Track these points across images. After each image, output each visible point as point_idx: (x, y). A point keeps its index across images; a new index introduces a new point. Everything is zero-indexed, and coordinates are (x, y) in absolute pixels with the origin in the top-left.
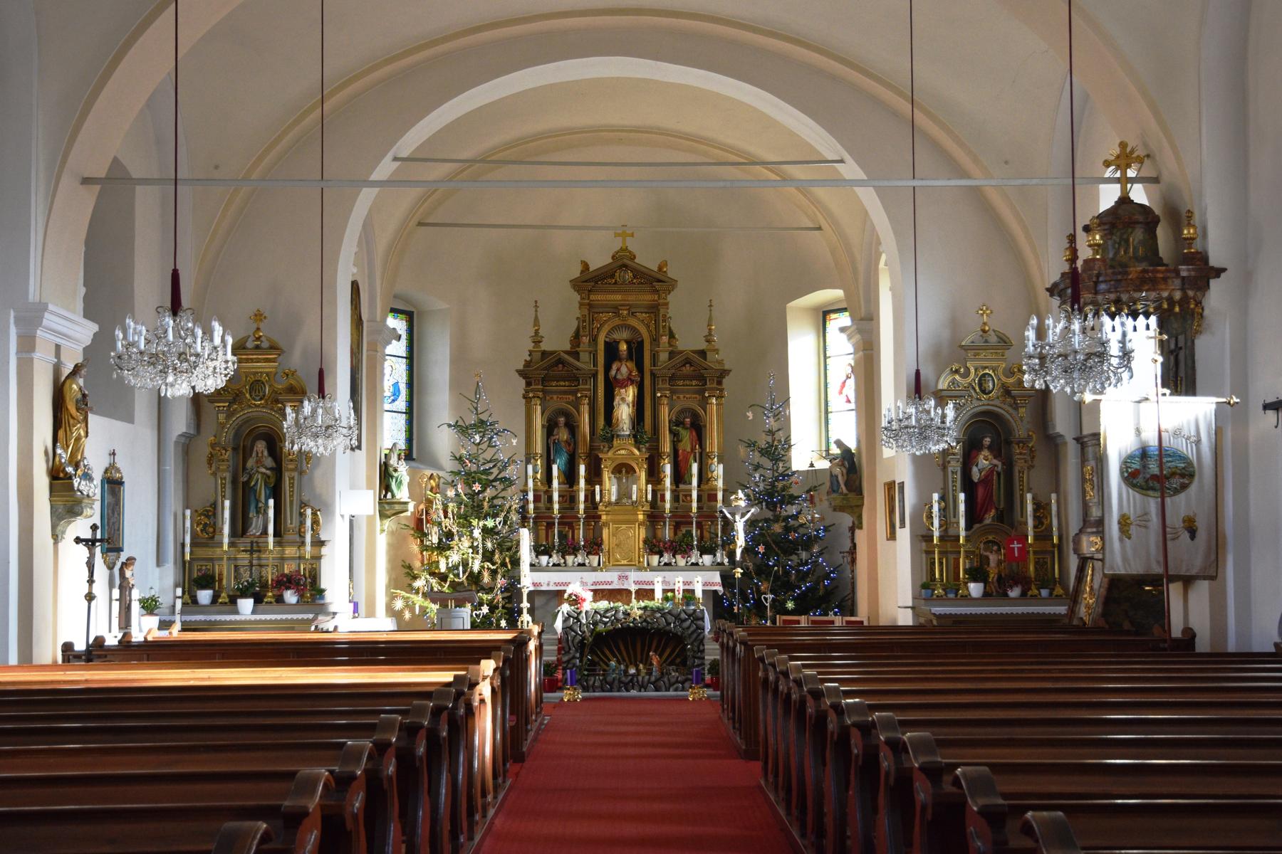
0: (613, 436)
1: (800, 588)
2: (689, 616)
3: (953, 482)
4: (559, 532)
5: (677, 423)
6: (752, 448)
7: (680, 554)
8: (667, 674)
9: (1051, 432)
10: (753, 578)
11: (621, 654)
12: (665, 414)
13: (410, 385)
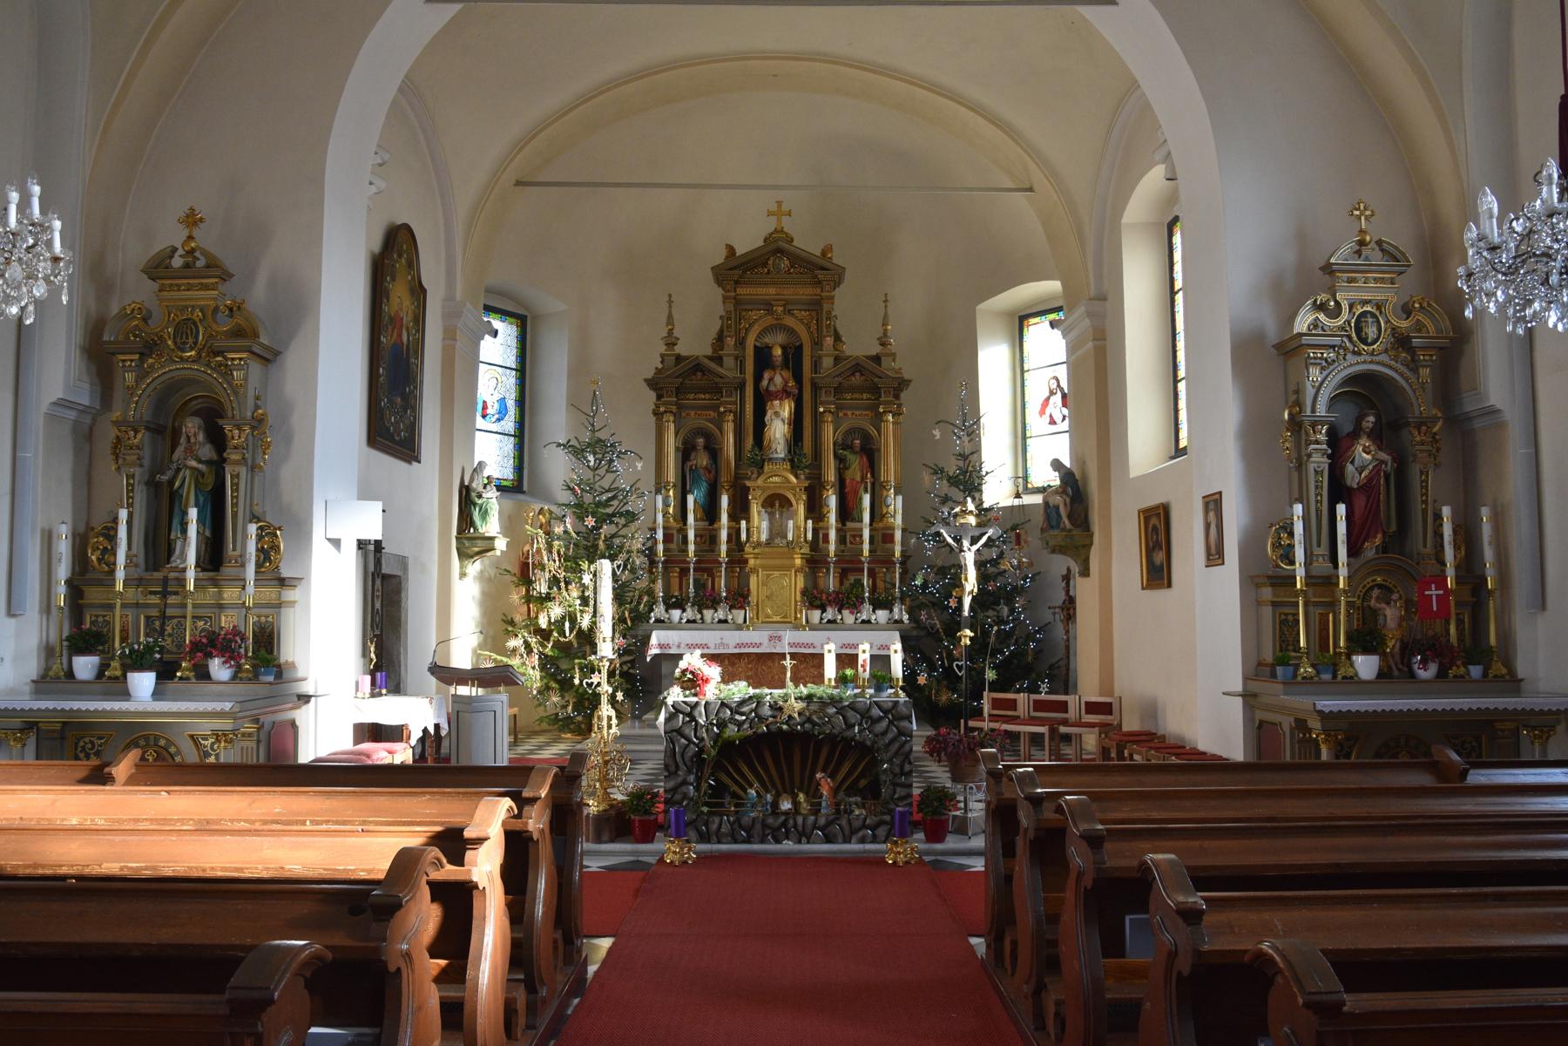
0: (763, 461)
1: (1002, 653)
2: (886, 712)
3: (1317, 487)
4: (695, 580)
5: (843, 445)
6: (939, 476)
7: (848, 608)
8: (845, 811)
9: (1468, 408)
10: (942, 640)
11: (767, 770)
12: (829, 434)
13: (521, 402)
